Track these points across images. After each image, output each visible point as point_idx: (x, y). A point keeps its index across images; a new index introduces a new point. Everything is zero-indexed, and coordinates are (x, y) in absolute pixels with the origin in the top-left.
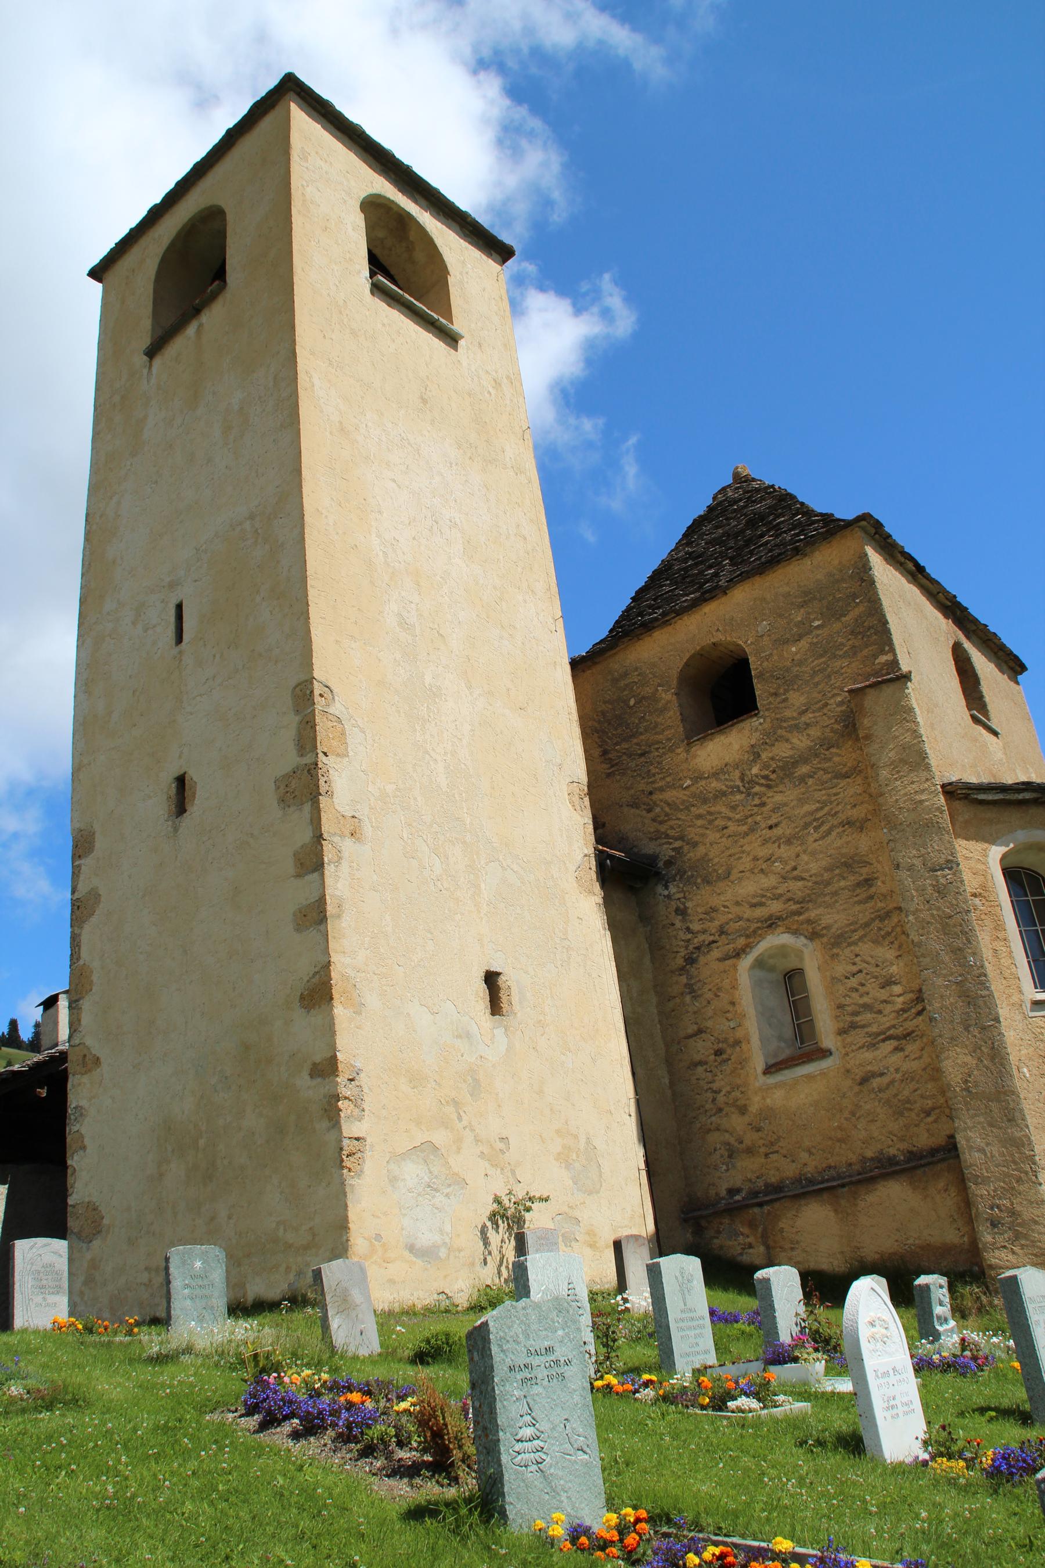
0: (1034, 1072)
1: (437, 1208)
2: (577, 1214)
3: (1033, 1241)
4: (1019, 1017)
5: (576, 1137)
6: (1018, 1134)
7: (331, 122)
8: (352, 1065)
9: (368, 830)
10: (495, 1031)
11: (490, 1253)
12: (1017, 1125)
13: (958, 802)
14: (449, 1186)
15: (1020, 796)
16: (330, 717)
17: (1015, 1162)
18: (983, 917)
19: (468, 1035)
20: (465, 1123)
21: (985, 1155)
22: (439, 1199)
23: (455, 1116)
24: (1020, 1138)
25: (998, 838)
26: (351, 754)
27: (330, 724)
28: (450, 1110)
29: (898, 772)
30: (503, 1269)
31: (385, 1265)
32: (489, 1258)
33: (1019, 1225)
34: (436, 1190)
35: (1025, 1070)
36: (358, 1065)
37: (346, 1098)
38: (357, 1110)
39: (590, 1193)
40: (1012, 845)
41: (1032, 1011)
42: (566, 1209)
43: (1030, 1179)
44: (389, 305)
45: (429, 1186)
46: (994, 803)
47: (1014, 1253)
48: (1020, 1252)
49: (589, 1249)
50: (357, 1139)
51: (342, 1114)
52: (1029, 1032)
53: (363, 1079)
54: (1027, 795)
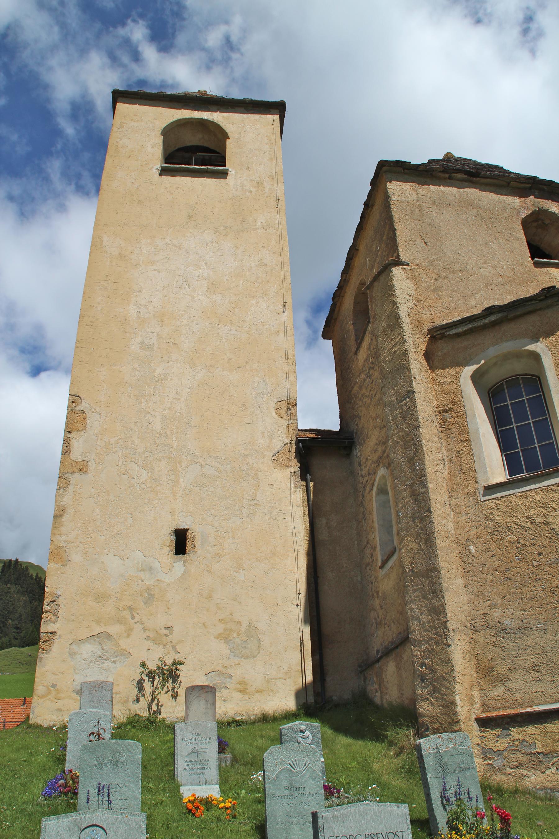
0: (481, 547)
1: (104, 669)
2: (229, 671)
3: (442, 695)
4: (472, 503)
5: (239, 623)
6: (437, 604)
7: (146, 99)
8: (54, 594)
9: (92, 466)
10: (174, 564)
11: (143, 695)
12: (437, 596)
13: (440, 341)
14: (117, 656)
15: (487, 321)
16: (77, 412)
17: (435, 628)
18: (450, 427)
19: (151, 569)
20: (136, 620)
21: (420, 622)
22: (107, 664)
23: (129, 617)
24: (438, 607)
25: (471, 359)
26: (88, 427)
27: (77, 415)
28: (126, 614)
29: (386, 335)
30: (154, 705)
31: (56, 701)
32: (142, 699)
33: (436, 681)
34: (106, 659)
35: (472, 547)
36: (59, 593)
37: (47, 611)
38: (55, 617)
39: (247, 657)
40: (483, 362)
41: (484, 495)
42: (220, 668)
43: (443, 642)
44: (173, 176)
45: (100, 657)
46: (465, 333)
47: (432, 704)
48: (435, 703)
49: (238, 693)
50: (52, 633)
51: (43, 620)
52: (480, 514)
53: (60, 601)
54: (493, 318)
